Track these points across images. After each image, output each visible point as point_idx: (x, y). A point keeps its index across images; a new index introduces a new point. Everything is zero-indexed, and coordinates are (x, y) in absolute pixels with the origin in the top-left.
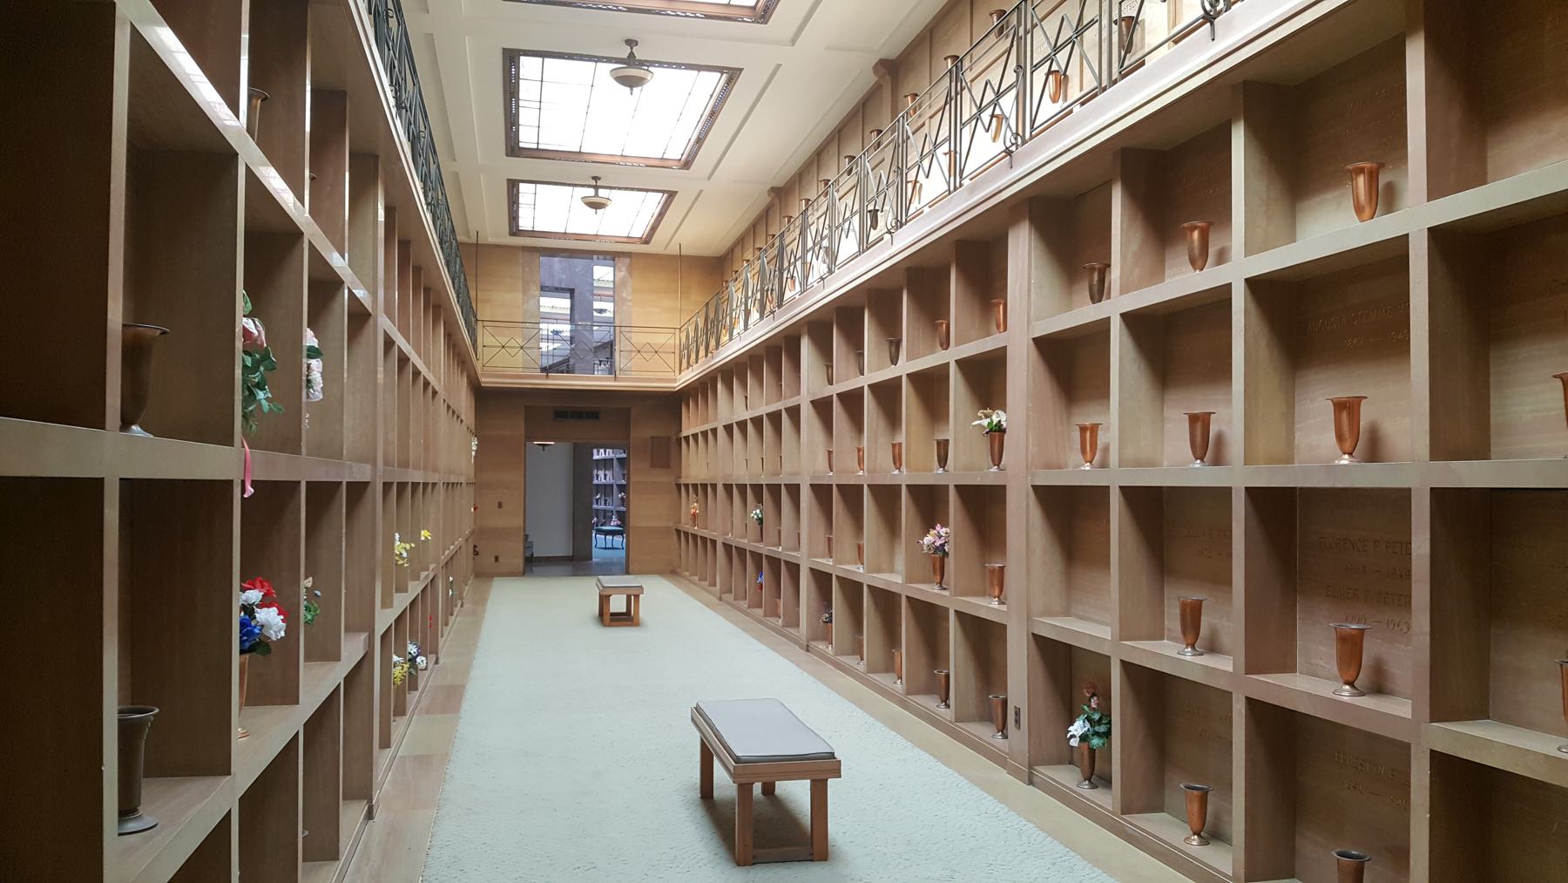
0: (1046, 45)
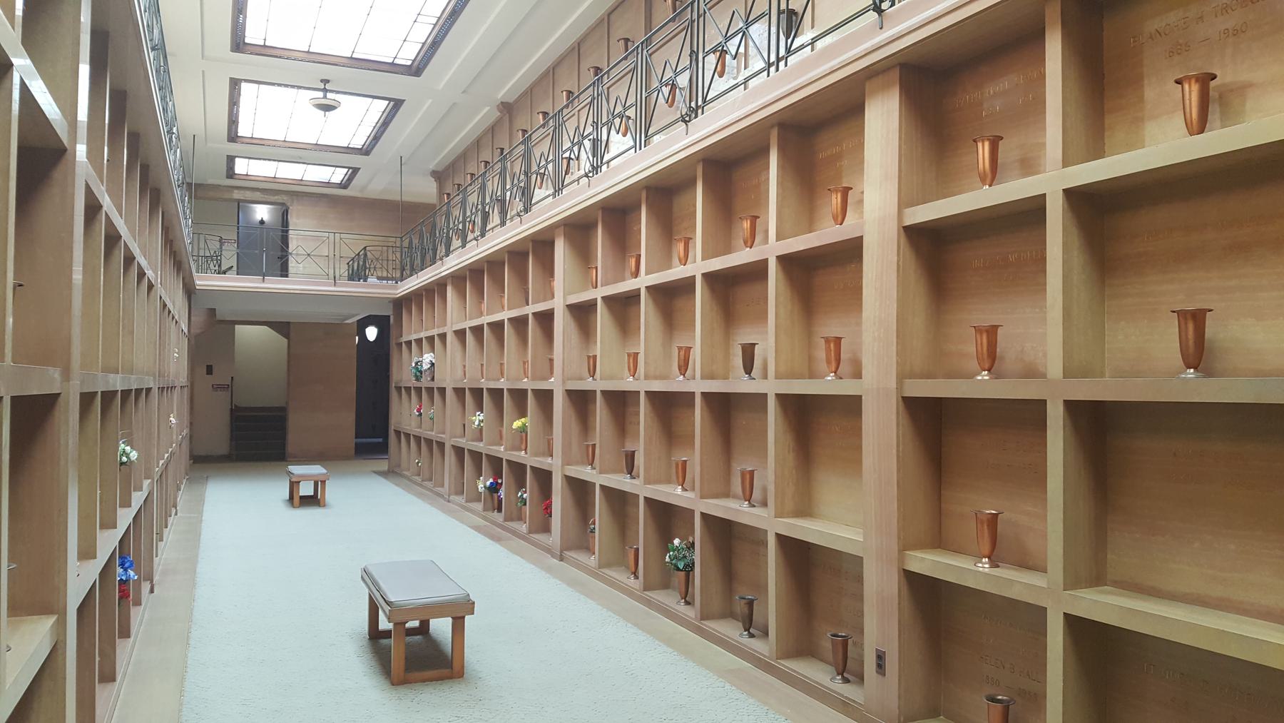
0: (569, 142)
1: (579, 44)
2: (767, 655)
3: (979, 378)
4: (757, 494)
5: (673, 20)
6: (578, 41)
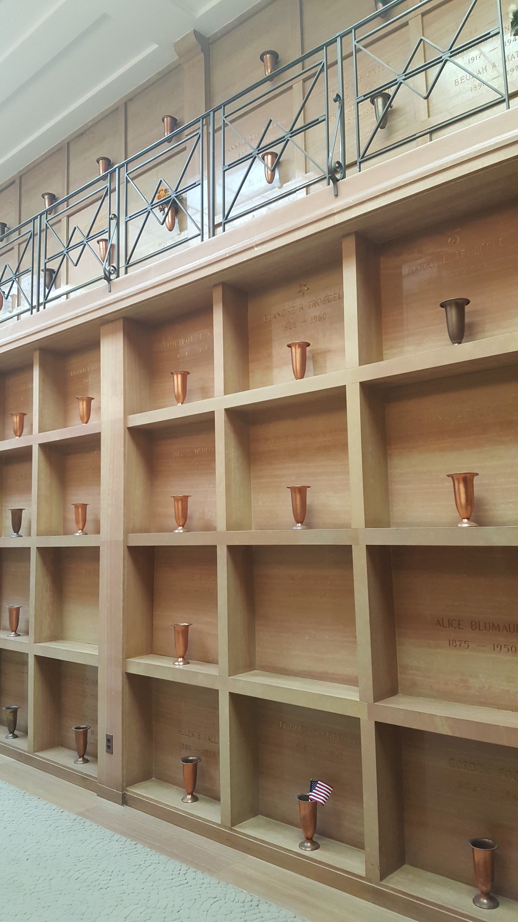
1: (21, 178)
2: (27, 750)
3: (177, 531)
4: (21, 625)
5: (169, 140)
6: (68, 141)
